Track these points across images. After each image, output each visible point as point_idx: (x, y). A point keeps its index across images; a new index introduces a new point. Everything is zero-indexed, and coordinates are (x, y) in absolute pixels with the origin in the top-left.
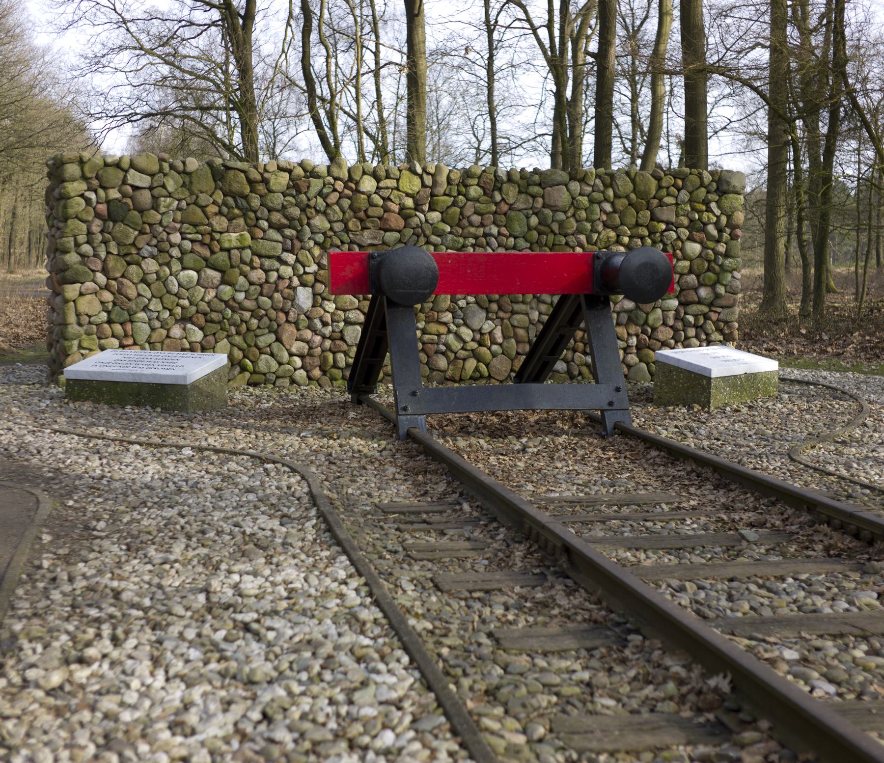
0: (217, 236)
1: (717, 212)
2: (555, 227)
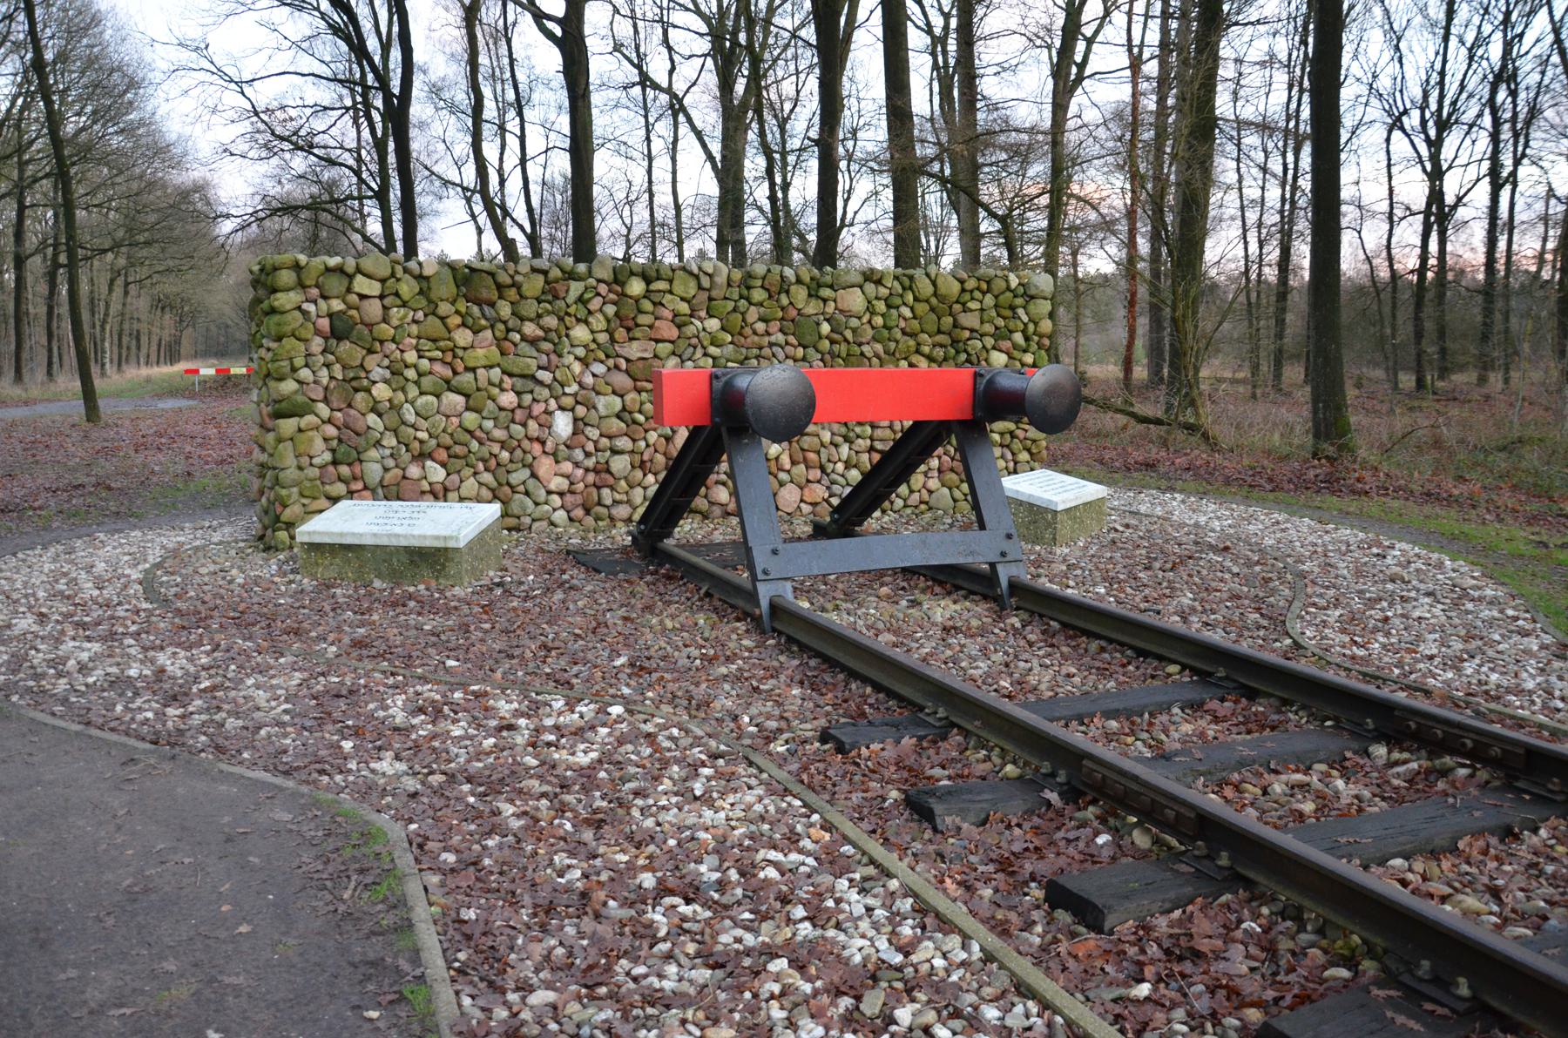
1: (1025, 318)
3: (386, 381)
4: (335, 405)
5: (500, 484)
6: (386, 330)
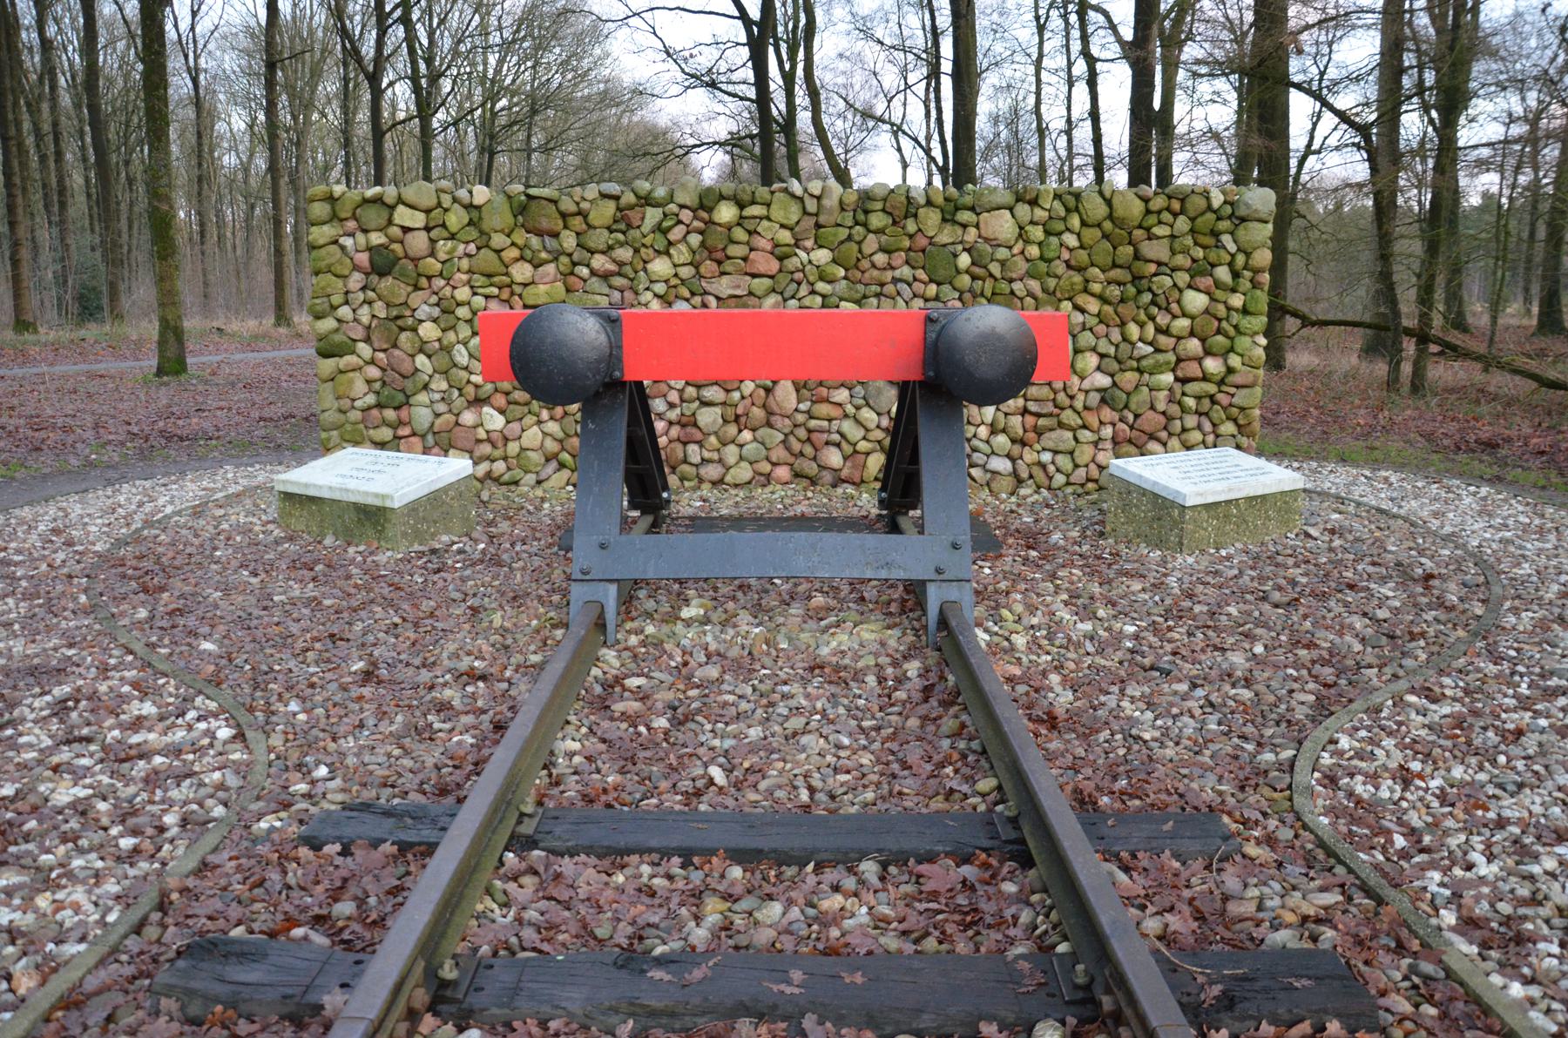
0: (518, 289)
1: (1232, 248)
2: (995, 268)
3: (435, 321)
4: (376, 345)
5: (568, 436)
6: (433, 265)
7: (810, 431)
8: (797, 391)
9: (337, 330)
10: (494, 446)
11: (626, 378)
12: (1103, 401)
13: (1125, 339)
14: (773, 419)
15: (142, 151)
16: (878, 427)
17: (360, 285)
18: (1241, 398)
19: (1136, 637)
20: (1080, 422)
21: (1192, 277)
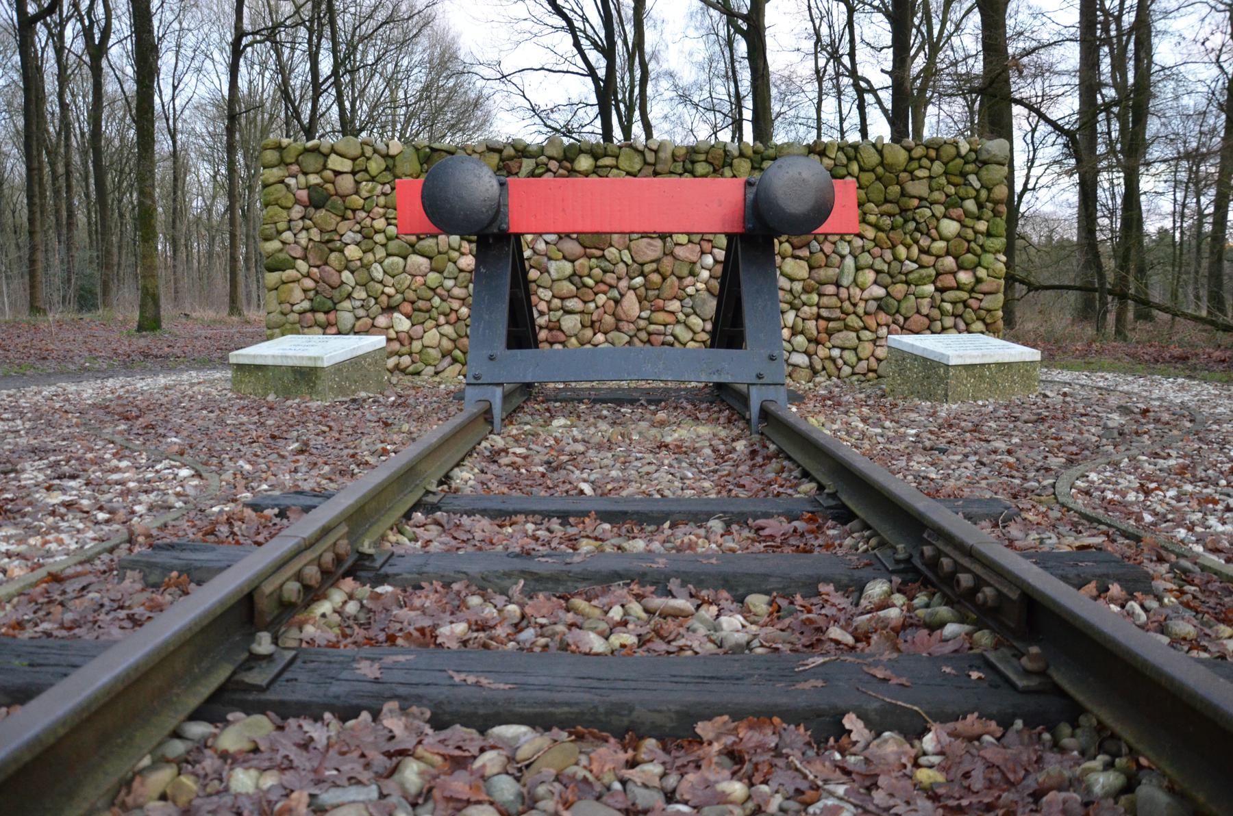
1: (977, 185)
3: (358, 244)
4: (311, 262)
5: (460, 336)
6: (357, 201)
7: (649, 334)
8: (640, 302)
9: (281, 250)
10: (402, 345)
11: (511, 230)
12: (880, 308)
13: (895, 258)
14: (621, 324)
15: (131, 195)
16: (703, 330)
17: (300, 215)
18: (987, 302)
19: (917, 435)
20: (861, 324)
21: (946, 209)
